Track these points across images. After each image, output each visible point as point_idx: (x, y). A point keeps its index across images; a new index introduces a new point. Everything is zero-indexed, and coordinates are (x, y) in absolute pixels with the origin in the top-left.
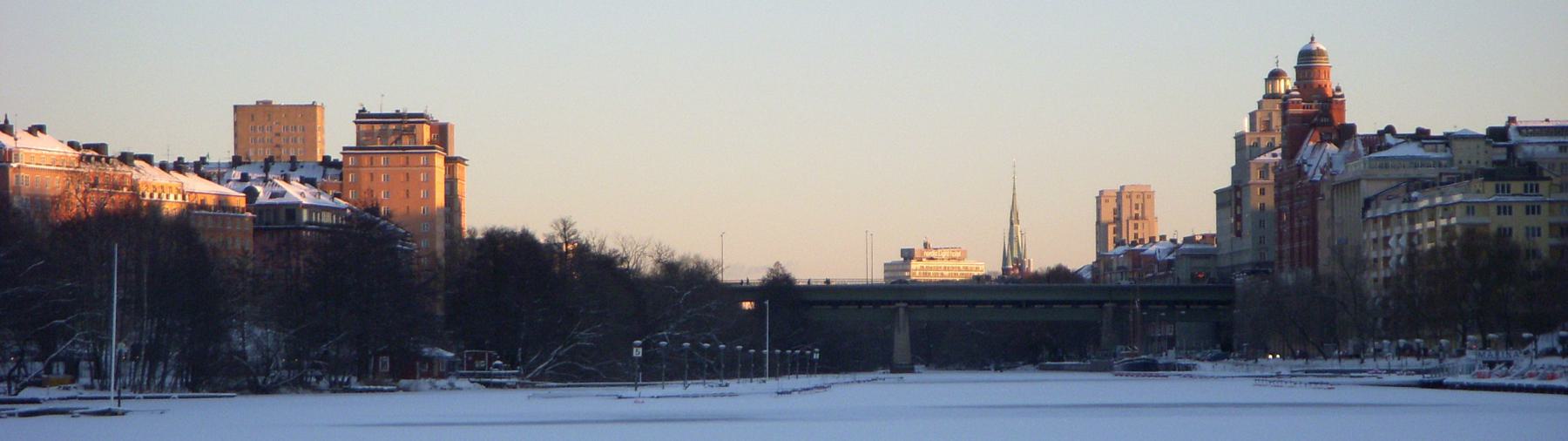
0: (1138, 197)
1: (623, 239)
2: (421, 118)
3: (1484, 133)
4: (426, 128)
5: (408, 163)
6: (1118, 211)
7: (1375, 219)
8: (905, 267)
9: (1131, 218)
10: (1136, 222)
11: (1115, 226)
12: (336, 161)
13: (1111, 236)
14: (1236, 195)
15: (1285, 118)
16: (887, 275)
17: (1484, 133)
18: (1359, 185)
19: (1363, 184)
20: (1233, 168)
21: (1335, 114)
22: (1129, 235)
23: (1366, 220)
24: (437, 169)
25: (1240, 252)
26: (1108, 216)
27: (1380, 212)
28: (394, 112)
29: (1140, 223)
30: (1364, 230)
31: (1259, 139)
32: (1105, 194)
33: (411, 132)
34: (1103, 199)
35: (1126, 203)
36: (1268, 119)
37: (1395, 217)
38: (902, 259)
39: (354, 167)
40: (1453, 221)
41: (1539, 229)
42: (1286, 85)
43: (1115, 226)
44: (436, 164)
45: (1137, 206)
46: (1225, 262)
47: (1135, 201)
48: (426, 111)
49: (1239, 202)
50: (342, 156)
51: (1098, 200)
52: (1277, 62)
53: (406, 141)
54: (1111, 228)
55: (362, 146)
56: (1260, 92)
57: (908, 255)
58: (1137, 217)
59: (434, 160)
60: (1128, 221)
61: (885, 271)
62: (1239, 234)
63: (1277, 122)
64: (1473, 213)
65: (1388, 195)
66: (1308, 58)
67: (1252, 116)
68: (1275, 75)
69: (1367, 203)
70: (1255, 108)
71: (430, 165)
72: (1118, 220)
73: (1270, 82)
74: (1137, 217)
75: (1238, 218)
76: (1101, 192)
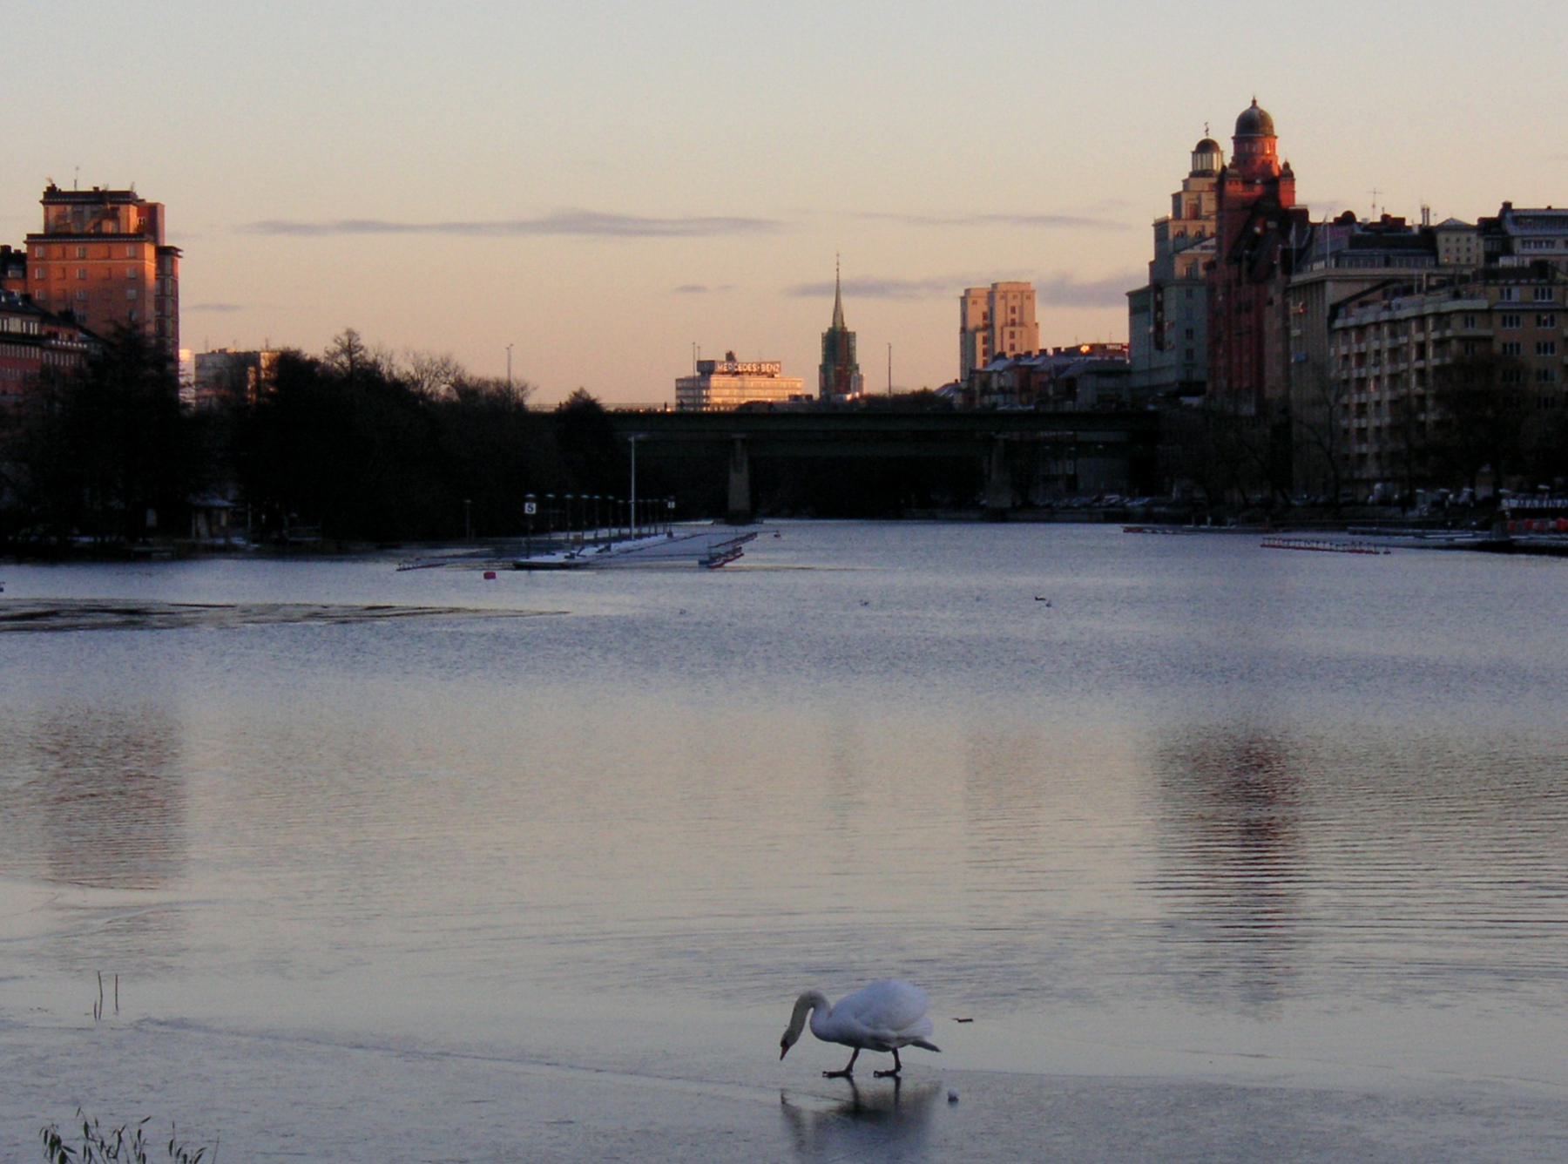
0: (1015, 297)
1: (415, 355)
2: (126, 197)
3: (1475, 223)
4: (133, 210)
5: (64, 254)
6: (989, 316)
7: (1345, 330)
8: (702, 384)
9: (1006, 325)
10: (1012, 329)
11: (985, 334)
12: (18, 252)
13: (980, 347)
14: (1155, 296)
15: (1220, 199)
16: (680, 393)
17: (1475, 223)
18: (1323, 287)
19: (1329, 286)
20: (1151, 264)
21: (1283, 197)
22: (1003, 344)
23: (1332, 332)
24: (147, 262)
25: (1159, 370)
26: (976, 320)
27: (1351, 322)
28: (92, 190)
29: (1017, 329)
30: (1330, 344)
31: (1185, 228)
32: (972, 293)
33: (113, 216)
34: (970, 301)
35: (1000, 306)
36: (1197, 202)
37: (1372, 330)
38: (697, 374)
39: (43, 259)
40: (1449, 333)
41: (1552, 345)
42: (1227, 153)
43: (985, 334)
44: (146, 257)
45: (1013, 310)
46: (1139, 381)
47: (1012, 303)
48: (132, 187)
49: (1159, 306)
50: (25, 246)
51: (964, 300)
52: (1207, 130)
53: (108, 227)
54: (980, 336)
55: (52, 235)
56: (1186, 168)
57: (707, 369)
58: (1013, 323)
59: (143, 252)
60: (1002, 328)
61: (678, 389)
62: (1160, 346)
63: (1209, 205)
64: (1473, 324)
65: (1360, 300)
66: (1253, 127)
67: (1177, 198)
68: (1206, 147)
69: (1335, 310)
70: (1180, 188)
71: (139, 256)
72: (989, 326)
73: (1199, 156)
74: (1013, 323)
75: (1159, 327)
76: (967, 291)
